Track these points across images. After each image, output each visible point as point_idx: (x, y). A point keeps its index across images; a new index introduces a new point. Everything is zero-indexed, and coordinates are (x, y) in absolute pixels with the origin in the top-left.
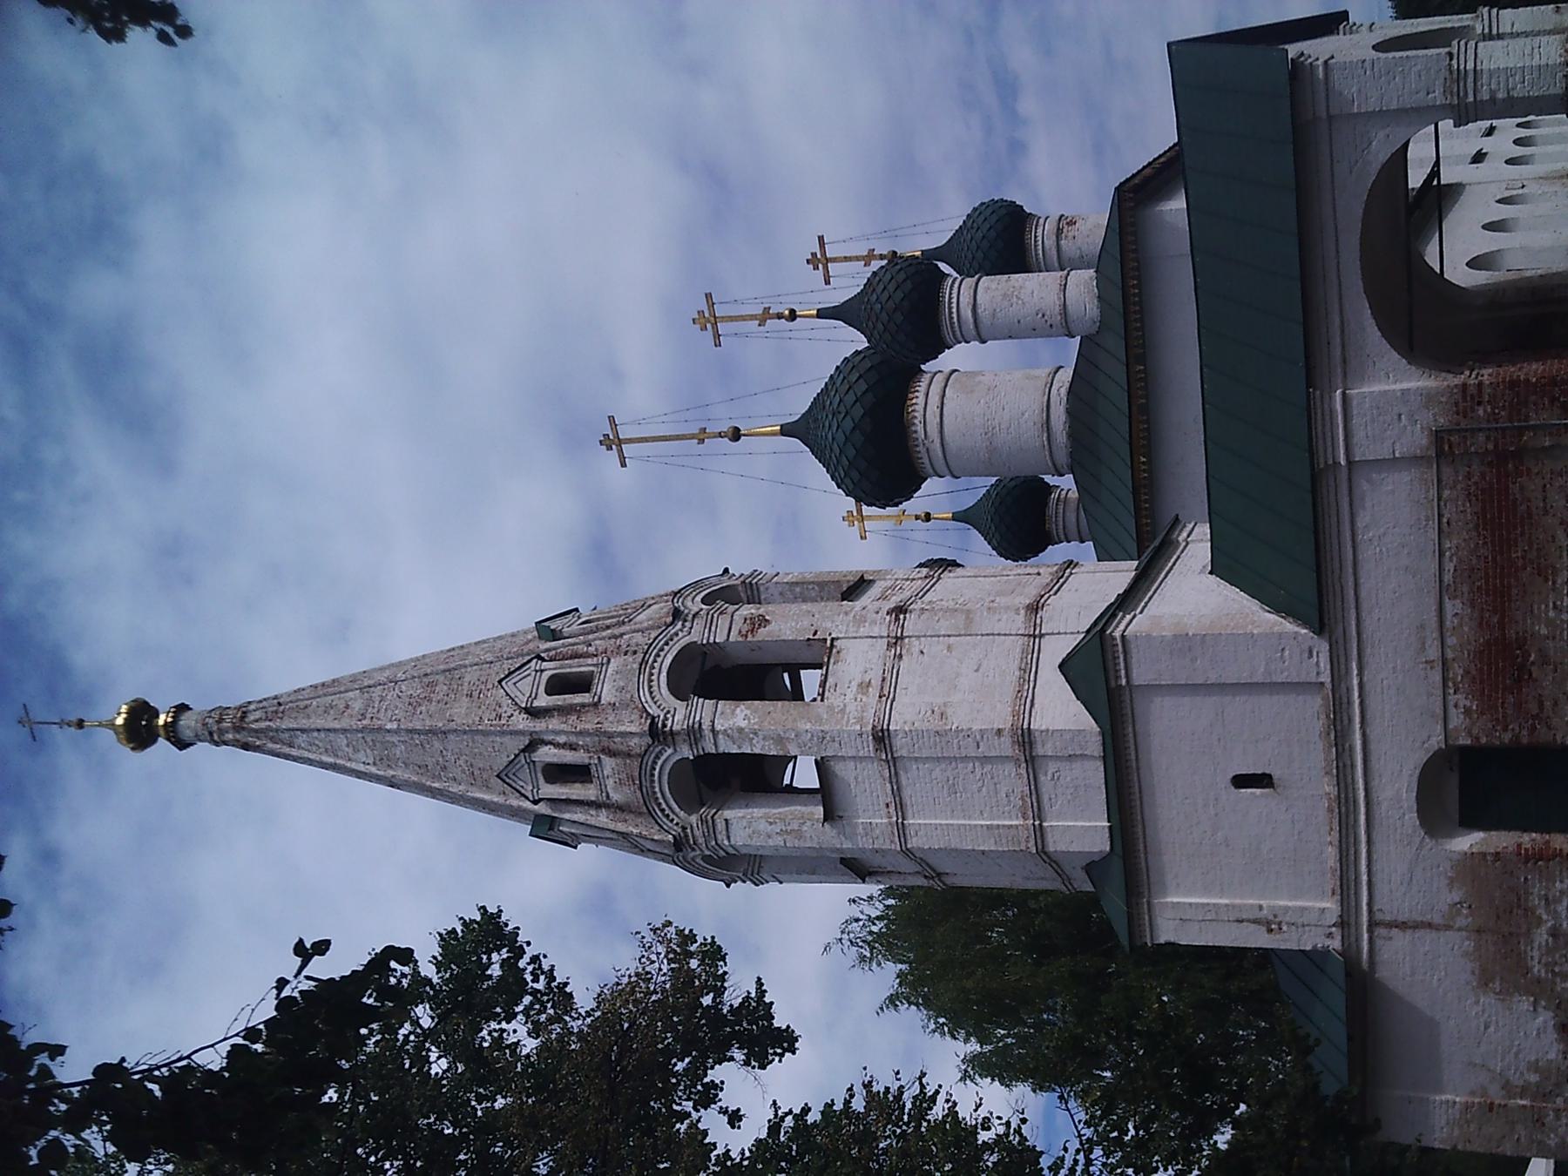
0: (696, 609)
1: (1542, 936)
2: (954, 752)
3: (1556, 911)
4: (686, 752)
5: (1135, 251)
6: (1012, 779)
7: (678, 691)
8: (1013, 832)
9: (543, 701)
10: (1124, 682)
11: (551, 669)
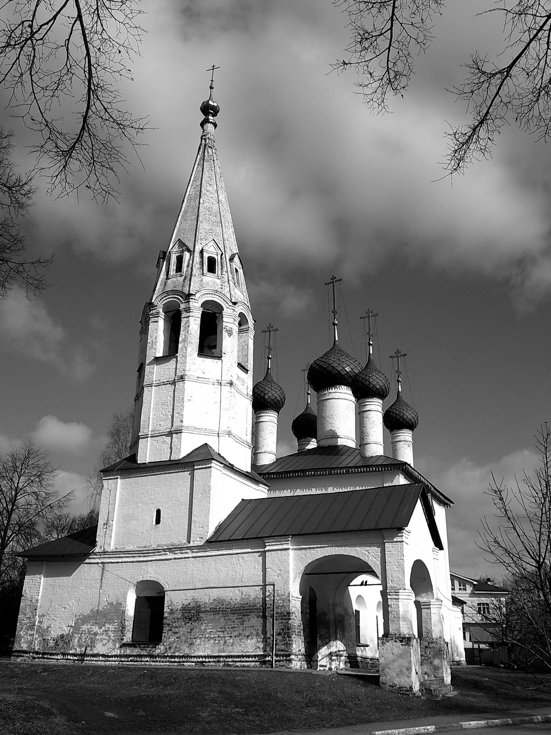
0: (236, 310)
1: (96, 629)
2: (175, 406)
3: (103, 634)
4: (182, 306)
5: (394, 469)
6: (165, 427)
7: (205, 304)
8: (147, 426)
9: (206, 255)
10: (195, 467)
11: (218, 258)
